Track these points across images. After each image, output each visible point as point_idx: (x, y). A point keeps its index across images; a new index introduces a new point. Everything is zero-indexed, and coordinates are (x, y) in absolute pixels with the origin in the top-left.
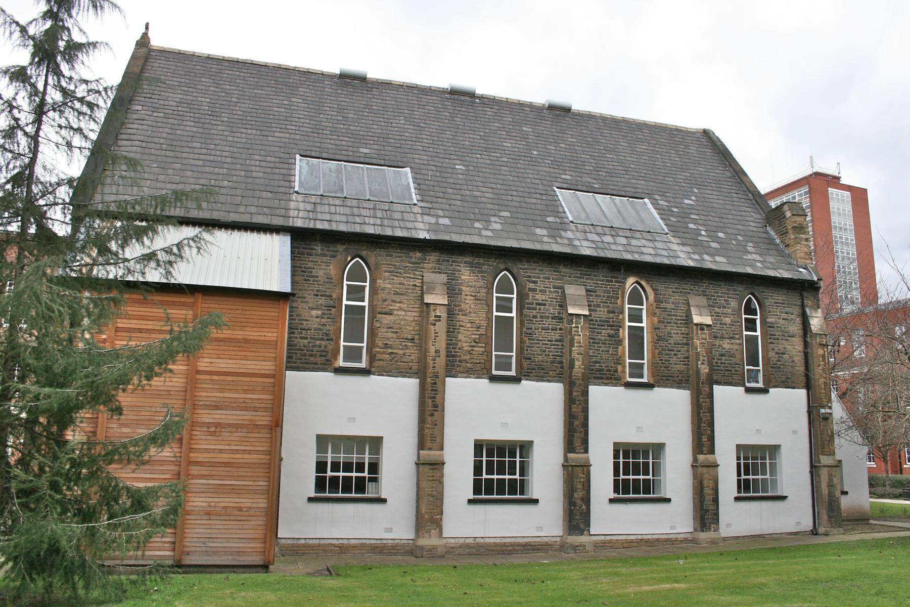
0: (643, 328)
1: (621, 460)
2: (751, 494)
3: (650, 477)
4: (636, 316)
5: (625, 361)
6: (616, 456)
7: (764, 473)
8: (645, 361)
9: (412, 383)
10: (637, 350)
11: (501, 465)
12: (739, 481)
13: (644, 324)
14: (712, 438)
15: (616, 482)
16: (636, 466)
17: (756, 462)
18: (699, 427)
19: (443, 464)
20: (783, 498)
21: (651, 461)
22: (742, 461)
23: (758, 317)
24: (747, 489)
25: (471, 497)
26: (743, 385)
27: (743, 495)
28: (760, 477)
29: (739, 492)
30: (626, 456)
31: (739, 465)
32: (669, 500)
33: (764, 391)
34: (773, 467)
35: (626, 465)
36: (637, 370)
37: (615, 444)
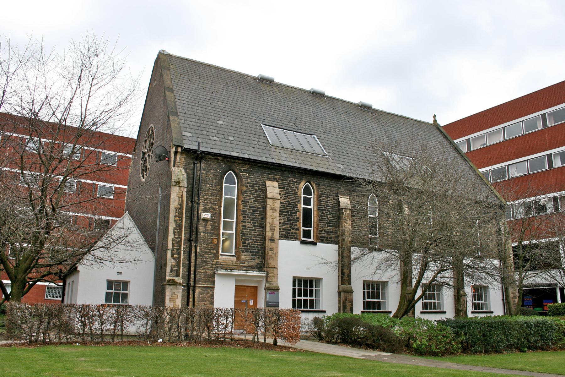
0: (311, 209)
1: (297, 288)
2: (428, 310)
3: (314, 298)
4: (307, 201)
5: (300, 228)
6: (294, 285)
7: (311, 295)
8: (312, 229)
9: (335, 247)
10: (307, 221)
11: (306, 291)
12: (364, 302)
13: (312, 207)
14: (349, 276)
15: (294, 301)
16: (306, 291)
17: (373, 290)
18: (342, 270)
19: (353, 292)
20: (445, 312)
21: (314, 288)
22: (366, 291)
23: (313, 197)
24: (426, 308)
25: (422, 311)
26: (368, 247)
27: (366, 310)
28: (308, 298)
29: (364, 308)
30: (300, 285)
31: (364, 292)
32: (445, 312)
33: (315, 244)
34: (383, 294)
35: (300, 290)
36: (307, 234)
37: (293, 277)
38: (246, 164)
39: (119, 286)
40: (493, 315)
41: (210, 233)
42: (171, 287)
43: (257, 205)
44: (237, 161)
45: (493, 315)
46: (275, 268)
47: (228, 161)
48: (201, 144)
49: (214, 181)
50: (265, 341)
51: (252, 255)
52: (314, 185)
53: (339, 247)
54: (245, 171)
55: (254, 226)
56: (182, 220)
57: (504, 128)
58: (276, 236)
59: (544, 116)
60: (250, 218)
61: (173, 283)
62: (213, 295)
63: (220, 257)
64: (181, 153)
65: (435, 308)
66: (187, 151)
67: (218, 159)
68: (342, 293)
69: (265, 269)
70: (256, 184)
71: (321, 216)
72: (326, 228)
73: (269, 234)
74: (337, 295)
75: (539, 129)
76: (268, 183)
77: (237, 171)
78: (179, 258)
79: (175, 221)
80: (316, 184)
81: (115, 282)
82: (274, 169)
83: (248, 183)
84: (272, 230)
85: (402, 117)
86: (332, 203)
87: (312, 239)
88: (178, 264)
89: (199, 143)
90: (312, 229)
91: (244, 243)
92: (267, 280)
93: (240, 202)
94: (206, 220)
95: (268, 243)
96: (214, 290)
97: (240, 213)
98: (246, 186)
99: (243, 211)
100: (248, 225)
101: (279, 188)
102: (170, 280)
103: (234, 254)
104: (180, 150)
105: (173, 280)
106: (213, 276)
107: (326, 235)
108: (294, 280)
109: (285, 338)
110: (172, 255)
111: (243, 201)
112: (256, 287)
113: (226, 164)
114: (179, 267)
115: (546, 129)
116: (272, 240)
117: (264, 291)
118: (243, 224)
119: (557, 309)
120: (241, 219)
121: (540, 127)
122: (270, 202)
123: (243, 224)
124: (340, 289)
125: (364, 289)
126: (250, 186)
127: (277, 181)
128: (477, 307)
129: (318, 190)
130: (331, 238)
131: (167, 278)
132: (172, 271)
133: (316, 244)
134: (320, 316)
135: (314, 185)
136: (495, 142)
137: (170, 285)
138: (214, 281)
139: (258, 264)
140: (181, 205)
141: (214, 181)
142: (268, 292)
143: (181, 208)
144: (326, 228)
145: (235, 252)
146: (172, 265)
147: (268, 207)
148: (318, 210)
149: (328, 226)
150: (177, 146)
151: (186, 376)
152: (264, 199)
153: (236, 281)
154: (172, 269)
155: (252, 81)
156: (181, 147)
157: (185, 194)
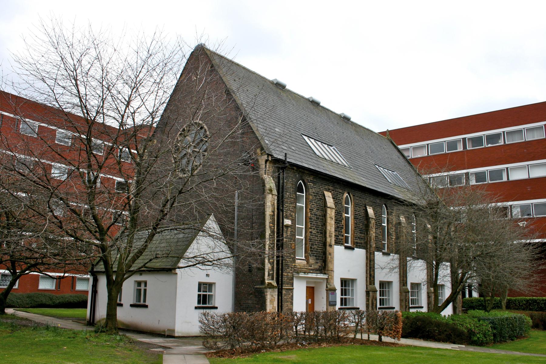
0: (349, 217)
13: (349, 216)
20: (216, 308)
25: (197, 305)
32: (216, 308)
38: (312, 175)
39: (205, 288)
40: (395, 310)
41: (290, 238)
42: (271, 290)
43: (319, 213)
44: (306, 172)
45: (395, 310)
47: (300, 171)
48: (288, 156)
49: (292, 190)
50: (369, 336)
51: (316, 259)
52: (352, 196)
53: (367, 251)
54: (311, 181)
55: (317, 232)
56: (274, 226)
57: (428, 145)
58: (333, 242)
59: (464, 139)
60: (314, 224)
61: (270, 286)
62: (292, 296)
63: (297, 261)
64: (271, 162)
65: (346, 305)
66: (276, 161)
67: (294, 169)
68: (371, 293)
69: (326, 272)
70: (318, 194)
71: (356, 224)
72: (359, 235)
74: (365, 294)
75: (458, 150)
76: (326, 193)
77: (306, 181)
78: (273, 262)
79: (270, 227)
80: (353, 196)
81: (203, 284)
82: (328, 180)
83: (313, 193)
84: (330, 236)
85: (368, 130)
86: (362, 213)
87: (349, 245)
88: (273, 267)
89: (286, 154)
91: (311, 248)
92: (327, 282)
93: (308, 211)
94: (287, 226)
95: (328, 248)
96: (292, 292)
98: (312, 195)
99: (310, 219)
101: (333, 198)
102: (269, 284)
103: (304, 258)
104: (270, 158)
105: (271, 283)
106: (292, 279)
107: (359, 241)
110: (269, 260)
111: (310, 209)
112: (313, 288)
113: (299, 173)
115: (465, 151)
116: (331, 246)
117: (325, 291)
118: (310, 230)
119: (472, 303)
121: (460, 148)
122: (329, 211)
123: (310, 230)
124: (369, 288)
126: (314, 196)
127: (331, 192)
129: (354, 199)
131: (267, 281)
132: (269, 275)
133: (353, 249)
135: (352, 196)
136: (419, 156)
137: (270, 288)
139: (320, 267)
141: (292, 190)
142: (330, 292)
143: (274, 215)
144: (359, 235)
145: (305, 256)
146: (269, 269)
147: (328, 216)
148: (354, 218)
149: (360, 233)
150: (268, 155)
152: (324, 207)
153: (307, 283)
155: (271, 86)
156: (271, 155)
157: (276, 202)
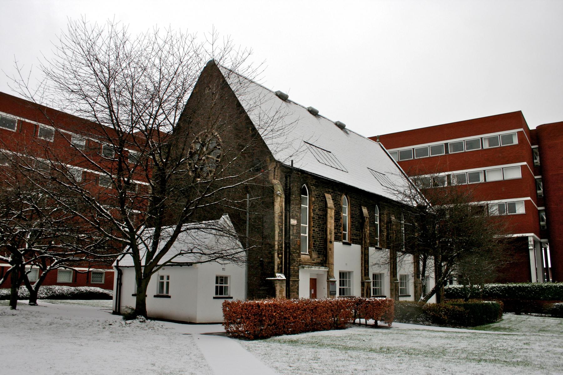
25: (215, 296)
29: (217, 293)
46: (333, 264)
58: (333, 239)
59: (446, 145)
62: (298, 287)
69: (327, 265)
73: (329, 237)
78: (282, 257)
80: (350, 197)
84: (331, 234)
90: (347, 232)
93: (311, 211)
95: (328, 243)
97: (312, 220)
100: (316, 230)
103: (307, 253)
108: (217, 278)
109: (381, 320)
114: (282, 265)
118: (313, 228)
120: (312, 224)
125: (168, 283)
128: (342, 292)
130: (357, 240)
132: (278, 269)
133: (350, 245)
134: (230, 301)
138: (298, 276)
140: (282, 212)
145: (309, 252)
148: (351, 217)
151: (554, 374)
154: (278, 267)
